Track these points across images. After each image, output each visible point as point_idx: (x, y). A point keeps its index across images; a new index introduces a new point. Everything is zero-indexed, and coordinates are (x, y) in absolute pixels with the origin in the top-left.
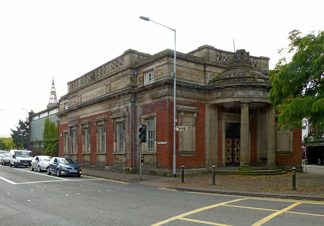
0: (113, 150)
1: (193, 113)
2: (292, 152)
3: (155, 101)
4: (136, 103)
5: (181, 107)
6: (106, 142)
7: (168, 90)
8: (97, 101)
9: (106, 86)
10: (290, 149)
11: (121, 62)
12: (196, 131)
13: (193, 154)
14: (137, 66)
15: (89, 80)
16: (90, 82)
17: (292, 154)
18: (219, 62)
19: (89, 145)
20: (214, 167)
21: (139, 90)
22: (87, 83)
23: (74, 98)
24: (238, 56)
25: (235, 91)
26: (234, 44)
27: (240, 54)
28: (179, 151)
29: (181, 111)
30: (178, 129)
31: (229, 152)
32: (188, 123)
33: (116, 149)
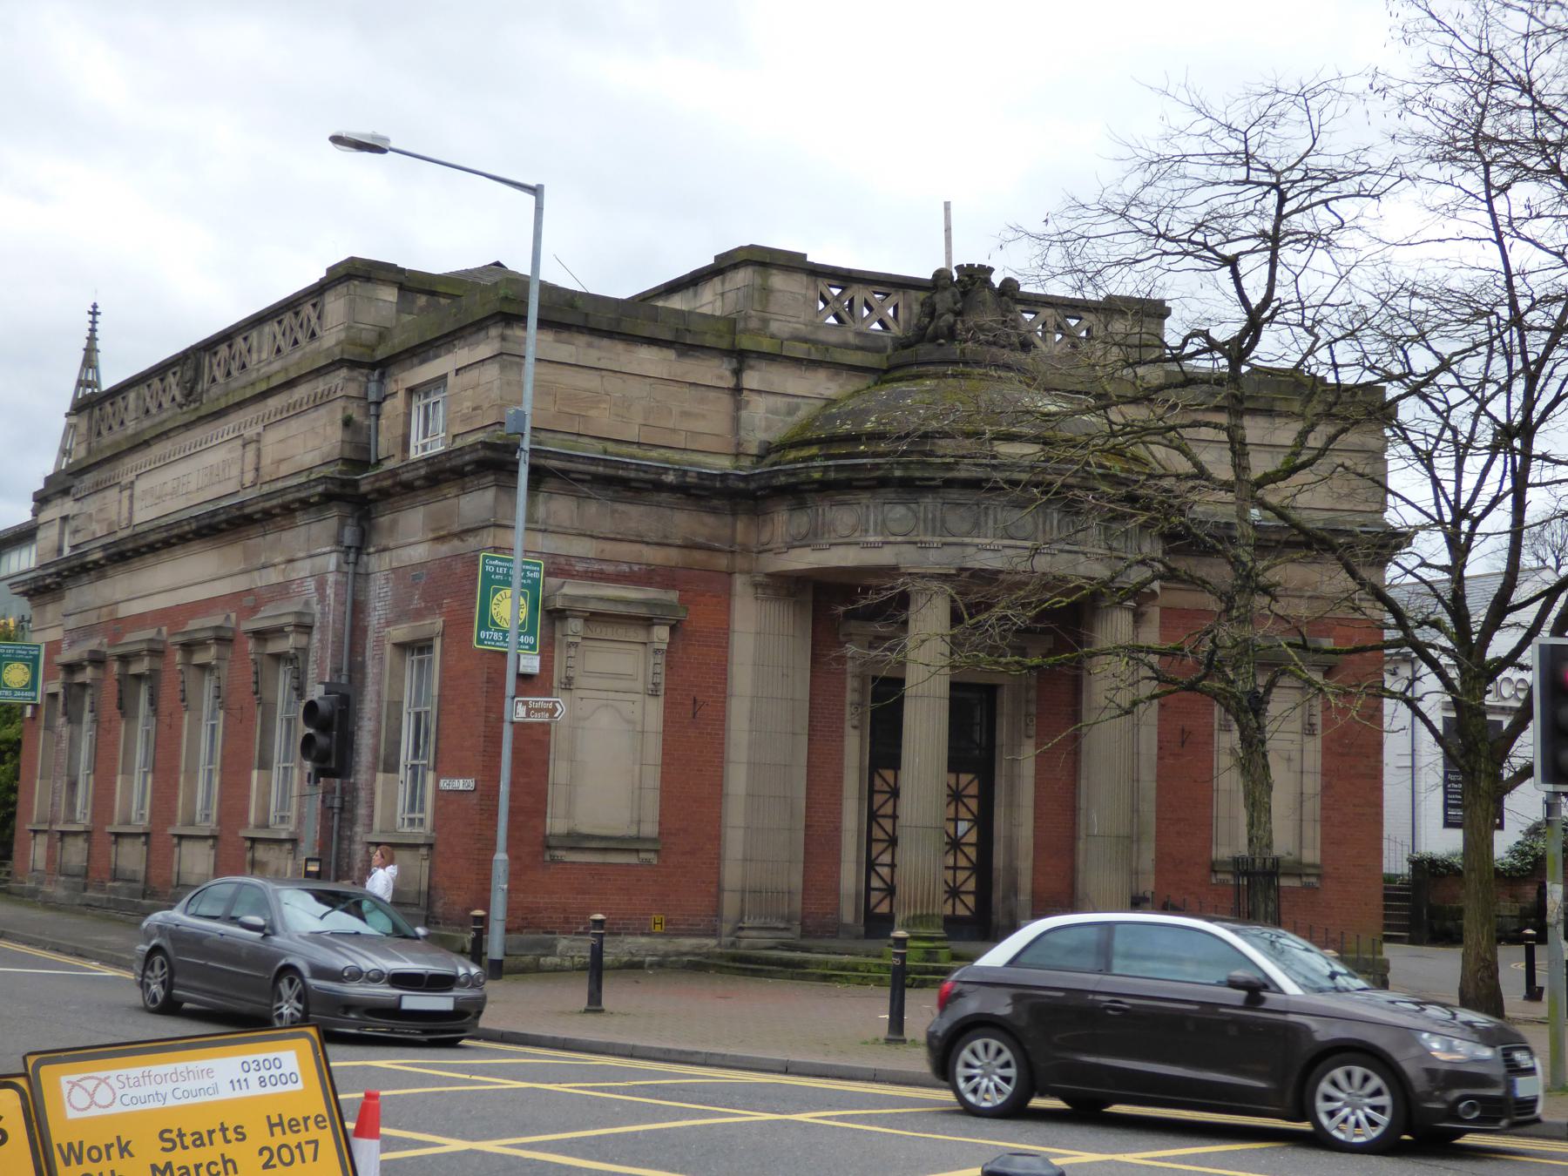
0: (246, 812)
1: (648, 623)
2: (1313, 866)
3: (445, 549)
4: (368, 554)
5: (572, 589)
6: (218, 767)
7: (496, 498)
8: (194, 526)
9: (244, 446)
10: (1301, 848)
11: (312, 323)
12: (668, 722)
13: (637, 851)
14: (380, 354)
15: (173, 399)
16: (179, 411)
17: (1313, 880)
18: (833, 338)
19: (423, 776)
20: (601, 921)
21: (377, 485)
22: (164, 416)
23: (100, 495)
24: (940, 308)
25: (875, 507)
26: (948, 230)
27: (954, 295)
28: (548, 832)
29: (564, 610)
30: (521, 711)
31: (960, 856)
32: (617, 676)
33: (265, 809)
